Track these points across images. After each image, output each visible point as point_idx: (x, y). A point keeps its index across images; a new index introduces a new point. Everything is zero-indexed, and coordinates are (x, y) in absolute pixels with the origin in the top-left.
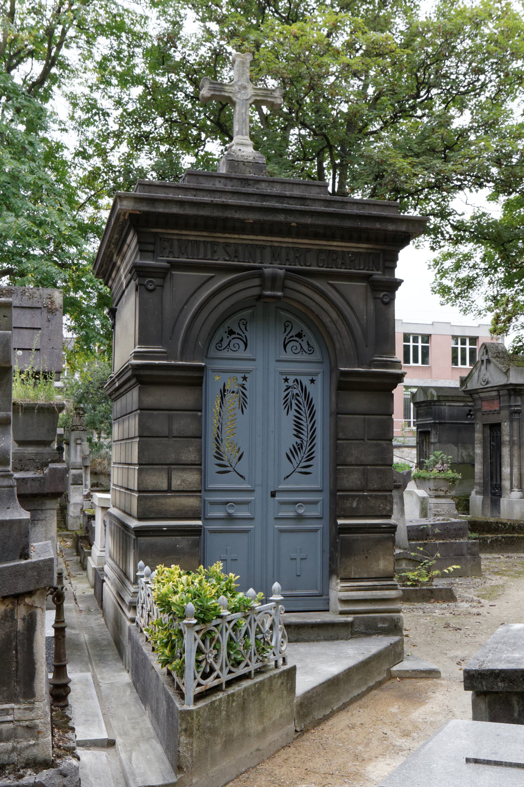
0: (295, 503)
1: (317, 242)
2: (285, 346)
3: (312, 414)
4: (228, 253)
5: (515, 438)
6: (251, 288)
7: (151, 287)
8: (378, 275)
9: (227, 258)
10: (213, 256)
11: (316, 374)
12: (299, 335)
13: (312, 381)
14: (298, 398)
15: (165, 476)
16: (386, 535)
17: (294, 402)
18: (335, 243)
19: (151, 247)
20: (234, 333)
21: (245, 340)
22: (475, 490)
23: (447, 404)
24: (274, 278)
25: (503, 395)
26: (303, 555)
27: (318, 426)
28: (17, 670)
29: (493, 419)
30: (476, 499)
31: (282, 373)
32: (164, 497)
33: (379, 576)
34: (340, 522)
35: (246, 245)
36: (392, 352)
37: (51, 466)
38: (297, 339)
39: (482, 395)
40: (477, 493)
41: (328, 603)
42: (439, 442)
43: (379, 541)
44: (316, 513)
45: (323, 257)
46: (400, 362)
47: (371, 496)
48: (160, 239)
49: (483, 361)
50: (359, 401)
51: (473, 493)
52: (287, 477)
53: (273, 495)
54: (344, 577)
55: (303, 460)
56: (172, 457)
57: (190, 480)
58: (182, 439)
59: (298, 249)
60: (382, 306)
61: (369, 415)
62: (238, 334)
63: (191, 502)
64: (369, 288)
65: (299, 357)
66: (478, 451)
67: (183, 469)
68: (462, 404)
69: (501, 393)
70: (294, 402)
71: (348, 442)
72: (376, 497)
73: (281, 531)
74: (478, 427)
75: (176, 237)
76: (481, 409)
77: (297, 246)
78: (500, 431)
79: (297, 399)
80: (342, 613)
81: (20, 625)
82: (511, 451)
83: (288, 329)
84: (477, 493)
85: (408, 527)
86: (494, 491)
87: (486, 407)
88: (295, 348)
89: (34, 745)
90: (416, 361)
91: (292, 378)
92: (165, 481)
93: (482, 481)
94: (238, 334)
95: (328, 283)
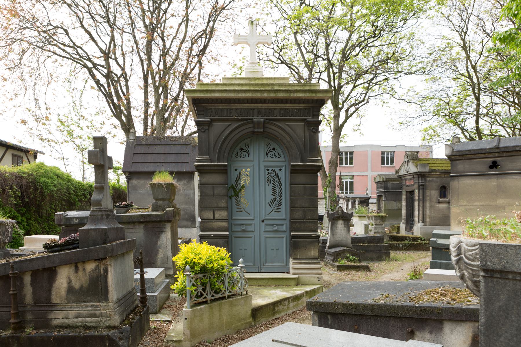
0: (273, 225)
1: (279, 105)
3: (280, 185)
5: (421, 198)
7: (203, 131)
8: (310, 119)
11: (282, 167)
12: (274, 149)
13: (280, 170)
15: (212, 213)
16: (314, 240)
17: (272, 180)
18: (288, 105)
19: (202, 113)
24: (259, 123)
28: (101, 289)
29: (410, 189)
30: (403, 226)
31: (265, 167)
34: (292, 233)
35: (245, 109)
37: (167, 209)
39: (406, 178)
40: (403, 223)
42: (387, 200)
45: (282, 112)
47: (307, 222)
50: (301, 178)
51: (401, 223)
53: (263, 221)
56: (215, 205)
59: (270, 109)
60: (312, 133)
63: (224, 224)
65: (274, 159)
66: (404, 204)
67: (220, 210)
70: (272, 180)
73: (266, 237)
74: (404, 193)
79: (273, 178)
80: (294, 274)
81: (102, 272)
82: (419, 204)
83: (268, 147)
84: (403, 223)
86: (410, 223)
87: (408, 183)
89: (109, 320)
90: (387, 163)
91: (270, 169)
92: (212, 215)
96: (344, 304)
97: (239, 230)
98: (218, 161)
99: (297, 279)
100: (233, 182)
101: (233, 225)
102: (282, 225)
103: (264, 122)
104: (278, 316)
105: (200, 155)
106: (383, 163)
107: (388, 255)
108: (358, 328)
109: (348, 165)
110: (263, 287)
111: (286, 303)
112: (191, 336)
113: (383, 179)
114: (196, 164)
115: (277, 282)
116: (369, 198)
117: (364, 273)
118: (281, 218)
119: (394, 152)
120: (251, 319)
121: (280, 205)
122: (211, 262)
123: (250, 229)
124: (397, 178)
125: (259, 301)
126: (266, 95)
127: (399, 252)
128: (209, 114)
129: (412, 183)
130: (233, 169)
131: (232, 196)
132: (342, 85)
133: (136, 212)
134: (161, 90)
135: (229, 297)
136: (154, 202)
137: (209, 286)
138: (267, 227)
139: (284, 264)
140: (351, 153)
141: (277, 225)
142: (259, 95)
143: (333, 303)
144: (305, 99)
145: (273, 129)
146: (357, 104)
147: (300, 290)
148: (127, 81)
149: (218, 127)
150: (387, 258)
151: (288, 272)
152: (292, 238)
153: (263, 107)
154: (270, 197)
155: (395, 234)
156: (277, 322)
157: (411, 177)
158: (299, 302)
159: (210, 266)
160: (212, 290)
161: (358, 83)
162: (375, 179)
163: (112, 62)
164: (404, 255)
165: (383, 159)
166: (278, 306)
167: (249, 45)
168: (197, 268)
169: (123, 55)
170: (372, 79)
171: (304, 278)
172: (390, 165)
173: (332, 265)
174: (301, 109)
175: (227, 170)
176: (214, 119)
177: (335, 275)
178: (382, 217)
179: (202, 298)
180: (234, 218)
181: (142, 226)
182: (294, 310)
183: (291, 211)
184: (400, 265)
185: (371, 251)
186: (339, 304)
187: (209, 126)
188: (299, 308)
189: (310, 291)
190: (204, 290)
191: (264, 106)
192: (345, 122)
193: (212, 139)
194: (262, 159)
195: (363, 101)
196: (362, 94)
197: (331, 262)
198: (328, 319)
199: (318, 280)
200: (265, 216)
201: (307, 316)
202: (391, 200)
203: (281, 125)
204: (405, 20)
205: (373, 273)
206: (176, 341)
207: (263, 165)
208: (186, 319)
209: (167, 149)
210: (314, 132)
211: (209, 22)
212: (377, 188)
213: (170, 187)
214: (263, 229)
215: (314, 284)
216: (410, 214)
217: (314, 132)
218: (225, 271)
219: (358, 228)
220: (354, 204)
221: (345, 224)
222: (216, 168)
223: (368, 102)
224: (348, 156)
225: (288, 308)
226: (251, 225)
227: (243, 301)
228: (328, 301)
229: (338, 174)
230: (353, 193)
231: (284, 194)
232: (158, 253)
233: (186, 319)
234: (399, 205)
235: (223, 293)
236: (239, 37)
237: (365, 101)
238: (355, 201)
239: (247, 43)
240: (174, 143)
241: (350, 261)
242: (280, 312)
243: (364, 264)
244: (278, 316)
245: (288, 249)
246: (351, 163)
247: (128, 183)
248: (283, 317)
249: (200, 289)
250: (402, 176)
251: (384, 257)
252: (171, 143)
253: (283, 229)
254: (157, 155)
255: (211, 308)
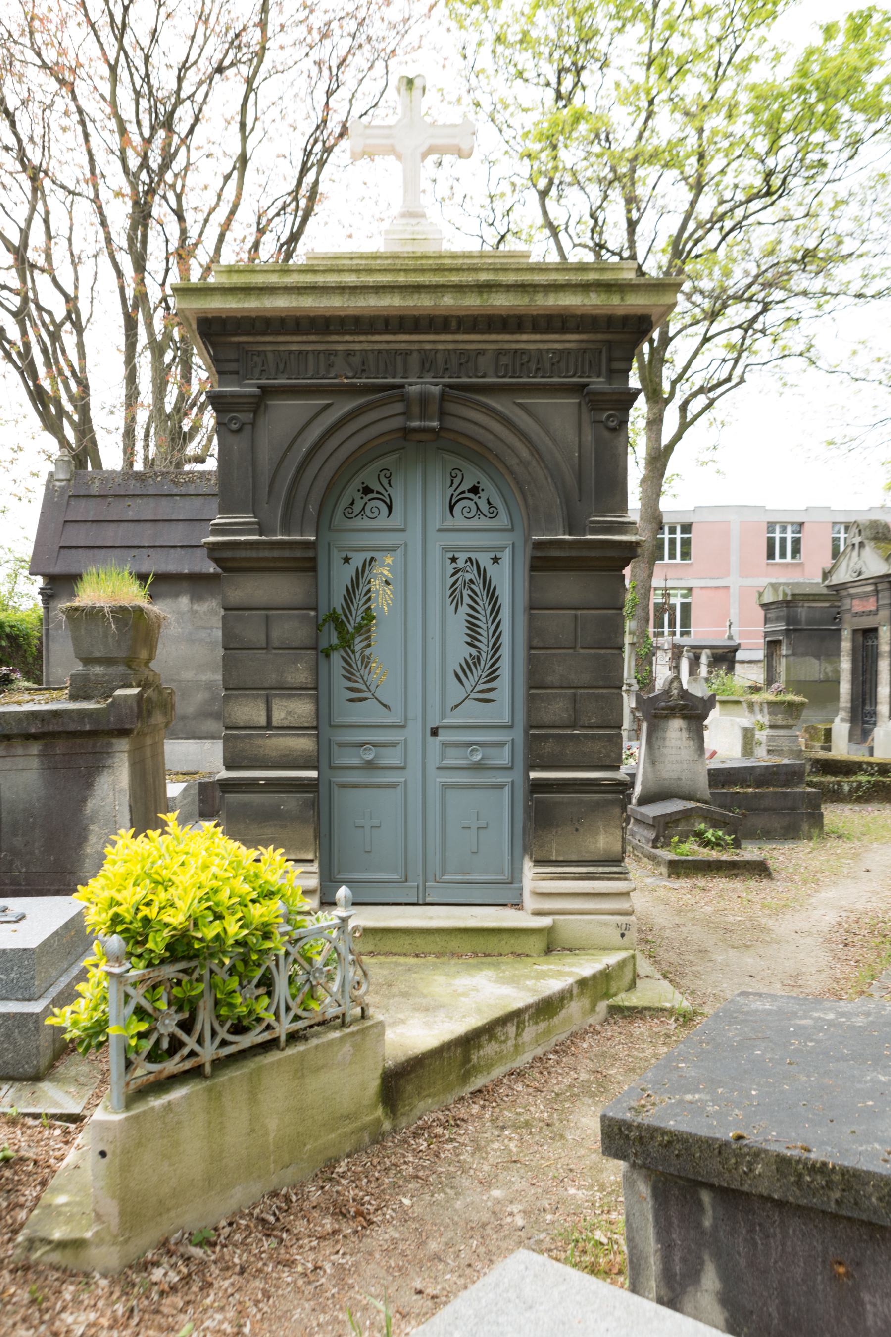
0: (469, 745)
1: (493, 337)
2: (452, 508)
3: (495, 610)
4: (350, 365)
6: (388, 418)
7: (234, 427)
8: (598, 383)
9: (350, 375)
10: (328, 372)
11: (502, 549)
12: (475, 490)
13: (496, 560)
14: (473, 586)
15: (263, 706)
16: (610, 796)
17: (466, 592)
18: (525, 337)
19: (233, 366)
20: (372, 491)
21: (388, 501)
22: (839, 716)
23: (806, 604)
24: (424, 399)
25: (883, 590)
26: (482, 823)
27: (505, 627)
29: (867, 623)
30: (841, 728)
31: (445, 549)
32: (262, 736)
33: (596, 858)
34: (533, 775)
35: (380, 351)
36: (622, 505)
37: (118, 692)
38: (471, 495)
39: (852, 591)
41: (521, 894)
42: (794, 654)
43: (597, 807)
44: (505, 760)
45: (504, 360)
46: (634, 523)
47: (585, 736)
48: (247, 352)
49: (854, 545)
50: (567, 587)
51: (837, 720)
52: (457, 706)
53: (434, 732)
54: (539, 858)
55: (481, 681)
56: (272, 679)
57: (299, 711)
58: (287, 651)
59: (462, 352)
60: (606, 434)
61: (583, 609)
62: (378, 492)
63: (303, 744)
64: (584, 409)
65: (475, 523)
66: (846, 664)
67: (290, 696)
68: (827, 604)
69: (880, 587)
70: (466, 592)
71: (549, 651)
72: (593, 737)
73: (446, 787)
75: (269, 348)
76: (850, 610)
77: (461, 346)
78: (877, 638)
79: (472, 588)
83: (457, 482)
84: (842, 720)
85: (709, 770)
86: (863, 717)
87: (858, 606)
88: (467, 509)
90: (783, 555)
91: (462, 557)
92: (263, 713)
93: (849, 705)
94: (378, 492)
95: (515, 403)
96: (783, 1163)
97: (355, 761)
98: (286, 530)
99: (549, 932)
100: (338, 601)
101: (335, 748)
102: (501, 745)
103: (443, 395)
104: (479, 1082)
105: (224, 509)
106: (771, 555)
107: (817, 819)
108: (848, 1274)
109: (678, 559)
110: (431, 959)
111: (511, 1029)
112: (122, 1223)
113: (785, 594)
114: (212, 539)
115: (480, 943)
116: (735, 649)
117: (752, 884)
118: (500, 877)
119: (801, 524)
120: (379, 1112)
121: (492, 677)
122: (219, 917)
123: (391, 758)
124: (825, 591)
125: (413, 1031)
126: (448, 300)
127: (840, 806)
128: (257, 371)
129: (871, 605)
130: (337, 557)
131: (332, 648)
132: (671, 334)
133: (19, 703)
134: (168, 356)
135: (293, 1037)
136: (79, 668)
137: (207, 1005)
138: (451, 751)
139: (505, 877)
140: (687, 528)
141: (481, 745)
142: (424, 302)
143: (726, 1144)
144: (582, 317)
145: (471, 418)
146: (711, 389)
147: (560, 974)
148: (79, 329)
149: (286, 414)
150: (815, 832)
151: (518, 905)
152: (532, 792)
153: (440, 347)
154: (460, 651)
155: (822, 755)
156: (475, 1109)
157: (870, 588)
158: (556, 1020)
159: (210, 932)
160: (222, 1025)
161: (715, 328)
162: (760, 594)
163: (42, 281)
164: (856, 817)
165: (771, 543)
166: (479, 1047)
167: (399, 157)
168: (157, 943)
169: (75, 262)
170: (755, 319)
171: (573, 927)
172: (789, 558)
173: (653, 858)
174: (568, 351)
175: (314, 559)
176: (273, 386)
177: (662, 893)
178: (791, 704)
179: (177, 1058)
180: (338, 720)
181: (35, 748)
182: (539, 1051)
183: (531, 700)
184: (856, 856)
185: (765, 809)
186: (757, 1154)
187: (255, 412)
188: (553, 1041)
189: (594, 977)
190: (186, 1026)
191: (444, 341)
192: (678, 437)
193: (266, 456)
194: (435, 523)
195: (728, 380)
196: (724, 361)
197: (648, 847)
198: (700, 1203)
199: (619, 932)
200: (443, 715)
201: (583, 1076)
202: (806, 654)
203: (499, 407)
204: (855, 143)
205: (779, 886)
206: (62, 1245)
207: (437, 542)
208: (103, 1154)
209: (165, 509)
210: (613, 430)
211: (304, 170)
212: (767, 621)
213: (129, 619)
214: (434, 759)
215: (606, 949)
216: (864, 694)
217: (613, 430)
218: (278, 944)
219: (725, 739)
220: (695, 662)
221: (689, 730)
222: (276, 553)
223: (742, 380)
224: (678, 536)
225: (516, 1046)
226: (393, 744)
227: (347, 1048)
228: (703, 1132)
229: (656, 582)
230: (688, 633)
231: (506, 639)
232: (85, 839)
233: (103, 1154)
234: (829, 669)
235: (269, 1027)
236: (368, 131)
237: (735, 380)
238: (697, 658)
239: (392, 151)
240: (183, 490)
241: (707, 844)
242: (489, 1066)
243: (751, 852)
244: (479, 1082)
245: (519, 826)
246: (686, 555)
247: (47, 609)
248: (499, 1083)
249: (169, 1025)
250: (843, 586)
251: (805, 827)
252: (175, 491)
253: (503, 757)
254: (130, 524)
255: (215, 1096)
